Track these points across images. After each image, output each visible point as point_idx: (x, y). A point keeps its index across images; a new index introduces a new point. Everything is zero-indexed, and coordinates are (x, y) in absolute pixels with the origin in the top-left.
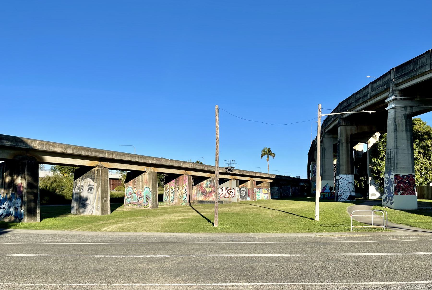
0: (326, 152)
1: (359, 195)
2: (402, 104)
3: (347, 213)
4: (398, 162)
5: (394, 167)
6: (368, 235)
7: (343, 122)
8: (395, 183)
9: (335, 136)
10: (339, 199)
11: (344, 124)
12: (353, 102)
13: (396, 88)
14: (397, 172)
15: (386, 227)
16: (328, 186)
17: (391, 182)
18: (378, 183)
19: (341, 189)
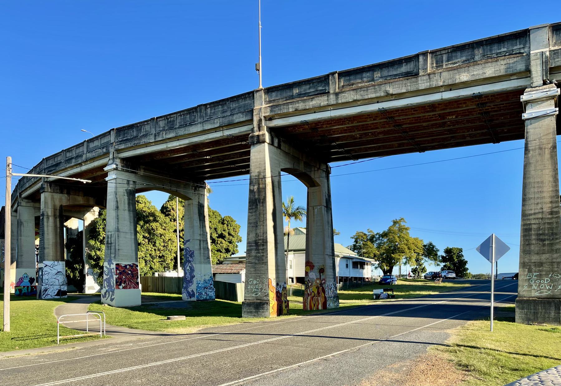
0: (23, 226)
1: (72, 287)
2: (125, 176)
3: (54, 317)
4: (120, 248)
5: (115, 254)
6: (81, 346)
7: (49, 187)
8: (116, 275)
9: (37, 205)
10: (44, 296)
11: (49, 191)
12: (62, 161)
13: (117, 155)
14: (118, 261)
15: (104, 332)
16: (27, 277)
17: (112, 272)
18: (97, 273)
19: (46, 281)
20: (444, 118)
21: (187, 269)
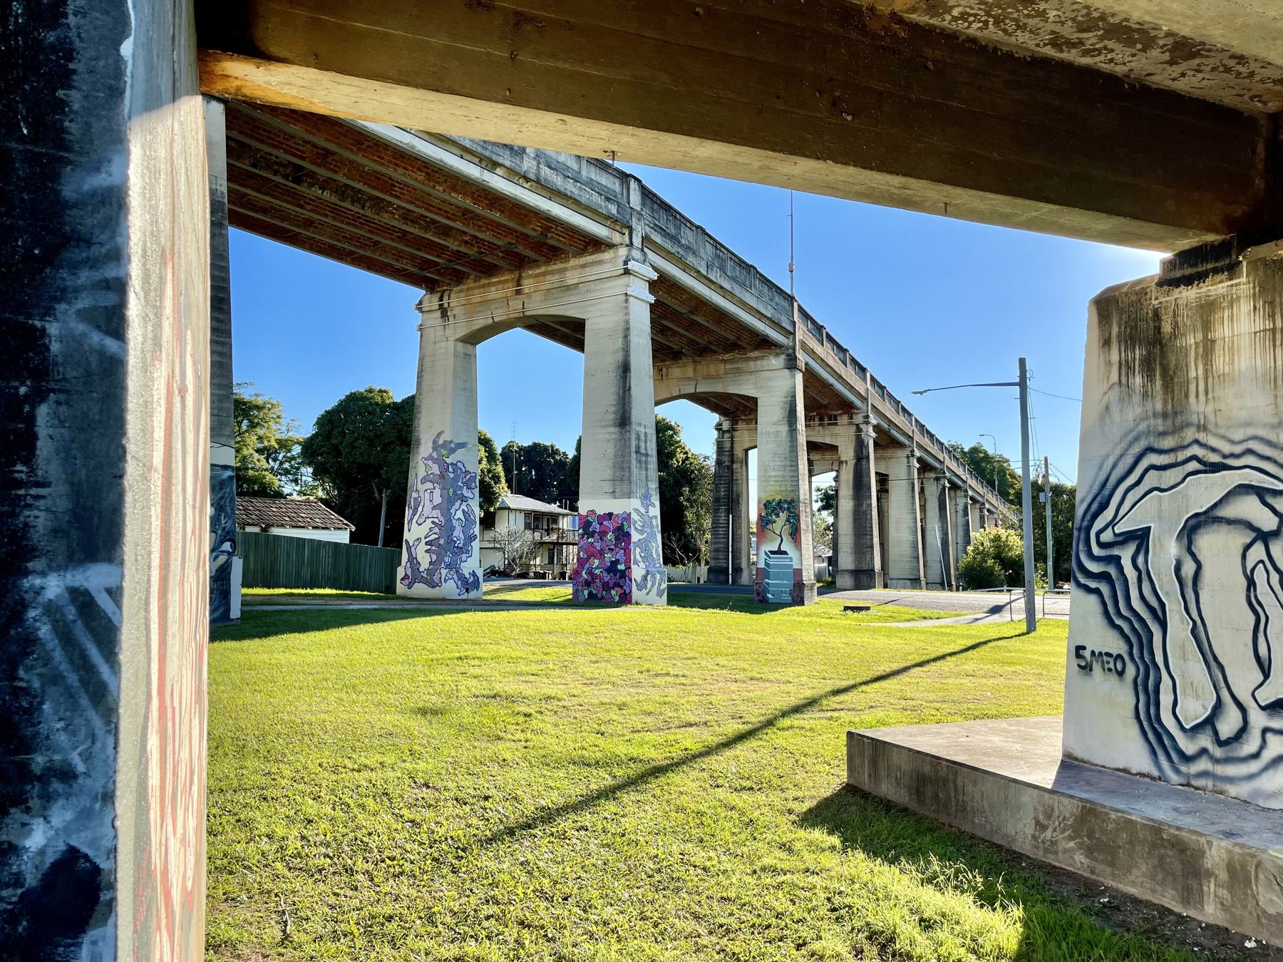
20: (298, 181)
21: (456, 517)
